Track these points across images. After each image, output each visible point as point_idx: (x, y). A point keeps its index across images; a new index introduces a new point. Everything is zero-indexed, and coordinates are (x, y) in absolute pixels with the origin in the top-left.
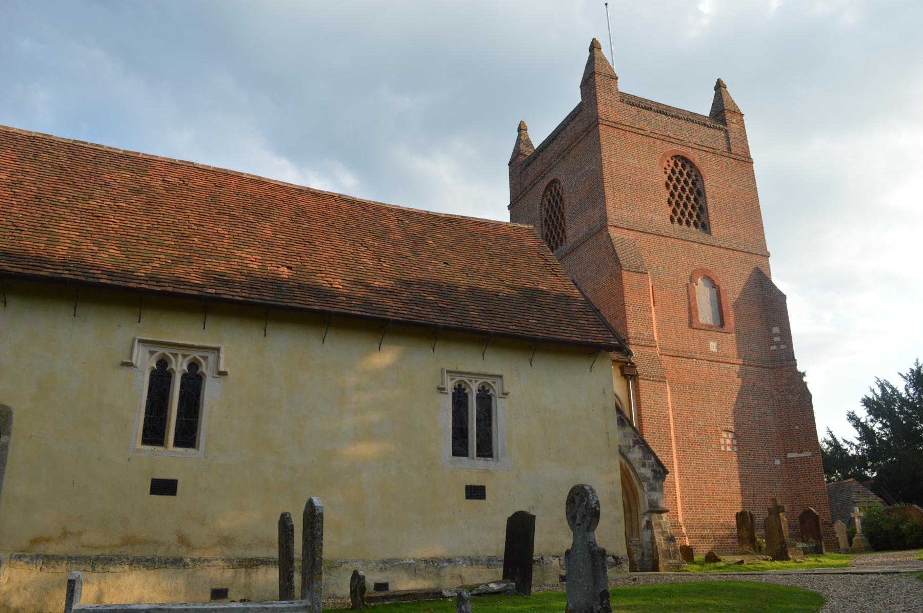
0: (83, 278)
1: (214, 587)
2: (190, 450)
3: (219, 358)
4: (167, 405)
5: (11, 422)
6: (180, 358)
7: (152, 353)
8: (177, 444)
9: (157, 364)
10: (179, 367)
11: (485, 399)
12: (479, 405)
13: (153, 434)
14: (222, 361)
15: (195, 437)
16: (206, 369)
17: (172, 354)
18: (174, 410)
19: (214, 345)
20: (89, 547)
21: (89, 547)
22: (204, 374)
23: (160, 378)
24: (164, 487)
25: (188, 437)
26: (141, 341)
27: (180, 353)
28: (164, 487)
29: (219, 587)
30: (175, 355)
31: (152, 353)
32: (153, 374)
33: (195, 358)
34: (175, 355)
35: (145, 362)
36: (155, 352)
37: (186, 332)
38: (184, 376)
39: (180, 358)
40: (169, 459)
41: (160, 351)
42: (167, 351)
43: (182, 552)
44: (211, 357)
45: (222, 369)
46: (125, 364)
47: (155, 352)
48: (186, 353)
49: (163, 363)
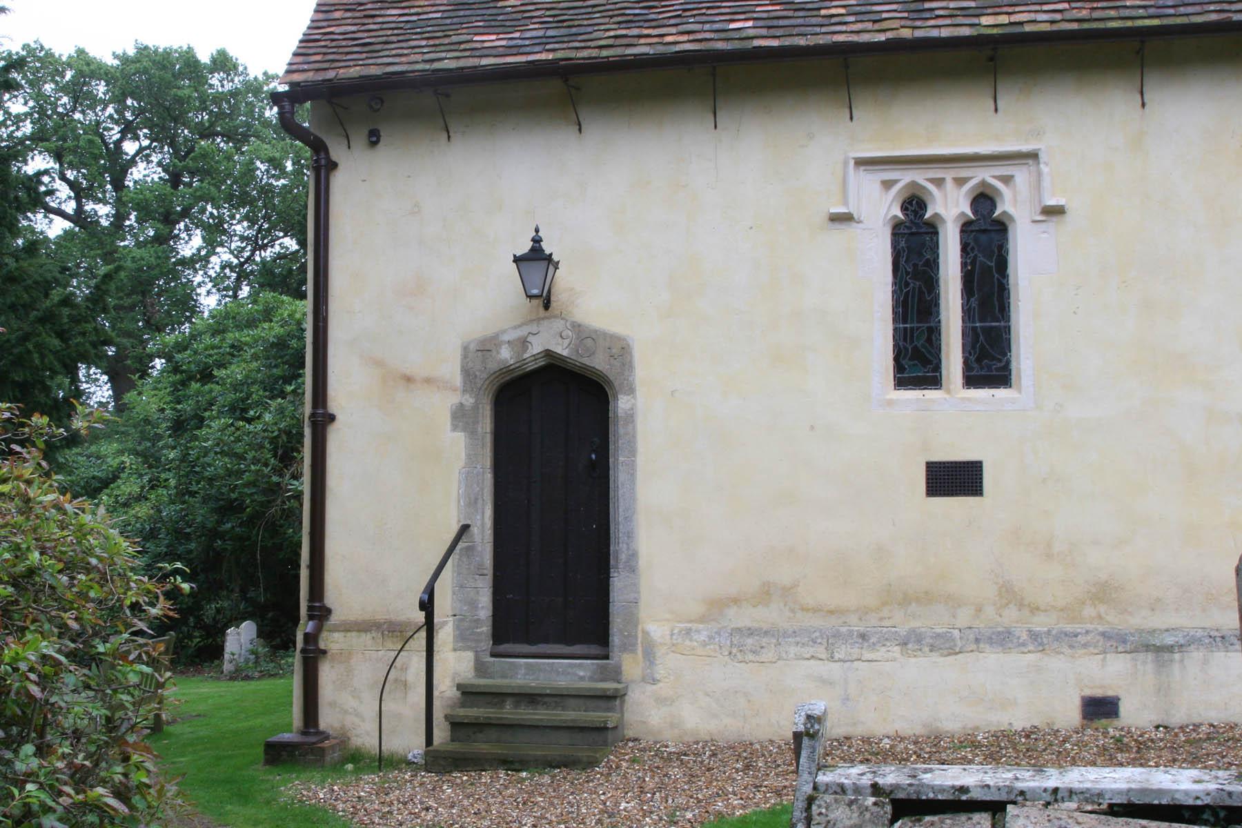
0: (720, 45)
1: (1088, 692)
2: (1001, 393)
3: (1039, 174)
4: (937, 297)
5: (631, 367)
6: (949, 184)
7: (887, 185)
8: (972, 381)
9: (904, 208)
10: (950, 207)
11: (988, 237)
12: (933, 335)
13: (915, 363)
14: (1046, 183)
15: (1008, 363)
16: (1015, 204)
17: (932, 181)
18: (952, 305)
19: (1025, 148)
20: (816, 610)
21: (816, 610)
22: (1011, 218)
23: (913, 239)
24: (954, 479)
25: (990, 363)
26: (861, 163)
27: (949, 174)
28: (954, 479)
29: (1098, 693)
30: (939, 182)
31: (887, 185)
32: (898, 231)
33: (984, 183)
34: (1007, 180)
35: (879, 207)
36: (895, 182)
37: (955, 124)
38: (967, 228)
39: (949, 184)
40: (954, 416)
41: (906, 177)
42: (919, 176)
43: (1010, 616)
44: (1021, 175)
45: (1051, 202)
46: (836, 219)
47: (895, 182)
48: (963, 173)
49: (914, 204)
